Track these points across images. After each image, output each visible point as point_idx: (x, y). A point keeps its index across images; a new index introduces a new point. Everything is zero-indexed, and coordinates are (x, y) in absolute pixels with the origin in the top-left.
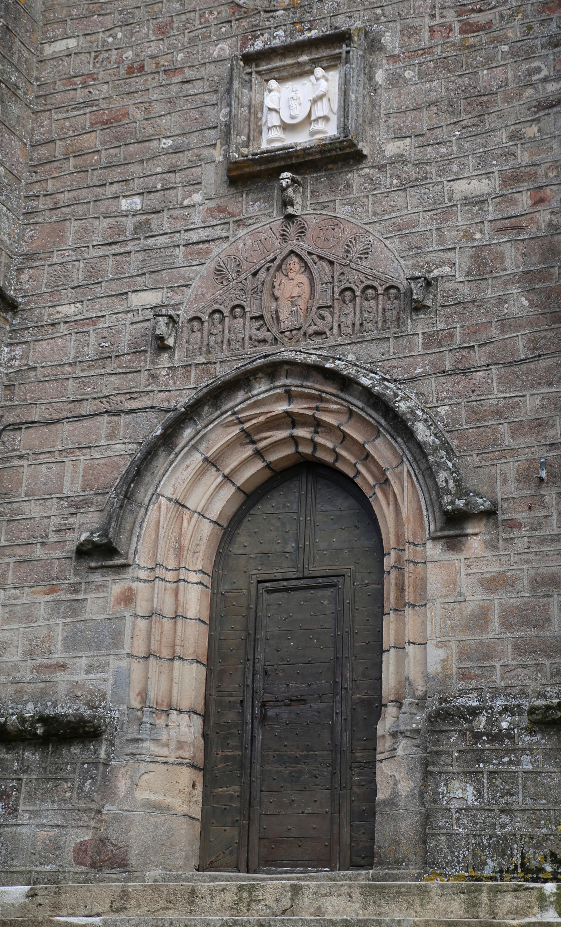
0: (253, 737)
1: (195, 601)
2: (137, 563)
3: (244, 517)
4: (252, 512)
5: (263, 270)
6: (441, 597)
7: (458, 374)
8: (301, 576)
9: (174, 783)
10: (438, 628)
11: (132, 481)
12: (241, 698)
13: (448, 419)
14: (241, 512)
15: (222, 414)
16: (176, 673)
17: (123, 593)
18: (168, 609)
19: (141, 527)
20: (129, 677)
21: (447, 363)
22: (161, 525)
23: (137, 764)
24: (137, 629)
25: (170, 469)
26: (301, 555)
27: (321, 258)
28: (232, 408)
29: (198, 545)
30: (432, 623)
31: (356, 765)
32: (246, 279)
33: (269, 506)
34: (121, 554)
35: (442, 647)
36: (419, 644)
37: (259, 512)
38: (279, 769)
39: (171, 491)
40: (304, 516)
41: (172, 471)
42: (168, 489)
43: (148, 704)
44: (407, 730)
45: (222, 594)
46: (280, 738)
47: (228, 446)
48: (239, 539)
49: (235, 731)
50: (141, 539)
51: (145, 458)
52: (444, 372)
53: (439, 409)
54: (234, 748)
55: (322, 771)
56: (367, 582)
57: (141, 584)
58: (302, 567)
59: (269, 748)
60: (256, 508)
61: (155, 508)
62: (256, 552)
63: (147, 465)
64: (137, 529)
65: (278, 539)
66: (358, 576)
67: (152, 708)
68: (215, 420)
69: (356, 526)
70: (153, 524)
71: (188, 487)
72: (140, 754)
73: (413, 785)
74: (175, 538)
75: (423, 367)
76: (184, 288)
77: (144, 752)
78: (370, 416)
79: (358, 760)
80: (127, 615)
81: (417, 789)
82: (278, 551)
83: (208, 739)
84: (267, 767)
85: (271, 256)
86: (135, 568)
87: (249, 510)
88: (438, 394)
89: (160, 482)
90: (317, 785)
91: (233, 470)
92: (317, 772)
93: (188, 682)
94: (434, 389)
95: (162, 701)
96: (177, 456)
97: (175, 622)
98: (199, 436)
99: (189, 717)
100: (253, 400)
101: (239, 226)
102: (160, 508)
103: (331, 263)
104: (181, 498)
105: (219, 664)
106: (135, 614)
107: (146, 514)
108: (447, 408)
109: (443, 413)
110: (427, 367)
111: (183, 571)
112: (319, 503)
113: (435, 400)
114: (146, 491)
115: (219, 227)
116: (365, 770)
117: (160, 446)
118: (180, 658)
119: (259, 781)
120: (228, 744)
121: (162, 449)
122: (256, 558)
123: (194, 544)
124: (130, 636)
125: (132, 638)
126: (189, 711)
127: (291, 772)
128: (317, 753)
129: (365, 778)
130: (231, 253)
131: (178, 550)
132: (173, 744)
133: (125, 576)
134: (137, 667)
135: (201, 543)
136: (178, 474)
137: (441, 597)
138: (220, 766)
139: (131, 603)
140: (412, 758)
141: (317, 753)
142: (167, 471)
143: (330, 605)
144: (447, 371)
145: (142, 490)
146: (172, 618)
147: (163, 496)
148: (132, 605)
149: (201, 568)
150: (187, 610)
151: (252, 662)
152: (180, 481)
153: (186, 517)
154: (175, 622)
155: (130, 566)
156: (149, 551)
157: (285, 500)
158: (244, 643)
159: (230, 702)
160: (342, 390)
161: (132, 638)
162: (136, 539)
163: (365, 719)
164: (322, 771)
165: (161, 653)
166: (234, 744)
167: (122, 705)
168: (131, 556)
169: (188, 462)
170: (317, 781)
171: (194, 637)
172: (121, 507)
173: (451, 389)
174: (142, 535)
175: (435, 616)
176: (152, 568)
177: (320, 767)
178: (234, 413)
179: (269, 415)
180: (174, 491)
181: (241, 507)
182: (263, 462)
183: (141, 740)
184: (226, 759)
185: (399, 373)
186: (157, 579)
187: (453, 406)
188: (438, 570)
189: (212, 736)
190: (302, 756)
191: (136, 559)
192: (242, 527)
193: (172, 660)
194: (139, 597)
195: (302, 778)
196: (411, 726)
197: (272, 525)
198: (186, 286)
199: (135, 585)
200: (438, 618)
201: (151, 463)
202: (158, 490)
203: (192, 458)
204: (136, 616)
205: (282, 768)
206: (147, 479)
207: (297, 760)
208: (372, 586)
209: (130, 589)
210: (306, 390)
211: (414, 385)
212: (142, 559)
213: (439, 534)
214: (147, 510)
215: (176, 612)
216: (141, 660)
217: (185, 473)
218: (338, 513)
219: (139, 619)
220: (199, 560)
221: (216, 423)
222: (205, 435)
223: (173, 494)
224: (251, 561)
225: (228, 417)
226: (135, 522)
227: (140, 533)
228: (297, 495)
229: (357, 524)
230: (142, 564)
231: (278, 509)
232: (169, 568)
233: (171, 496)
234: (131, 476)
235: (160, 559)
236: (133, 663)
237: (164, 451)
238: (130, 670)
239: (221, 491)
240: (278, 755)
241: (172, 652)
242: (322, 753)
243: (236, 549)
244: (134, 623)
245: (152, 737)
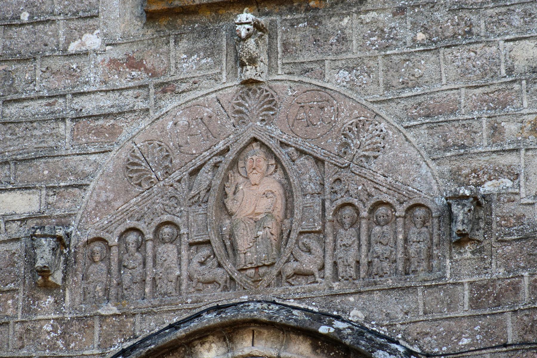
5: (208, 167)
7: (527, 350)
21: (510, 331)
27: (302, 153)
32: (179, 181)
52: (505, 345)
75: (472, 336)
76: (77, 191)
85: (221, 146)
101: (164, 92)
103: (318, 161)
110: (478, 337)
115: (130, 92)
130: (154, 136)
144: (511, 345)
198: (80, 186)
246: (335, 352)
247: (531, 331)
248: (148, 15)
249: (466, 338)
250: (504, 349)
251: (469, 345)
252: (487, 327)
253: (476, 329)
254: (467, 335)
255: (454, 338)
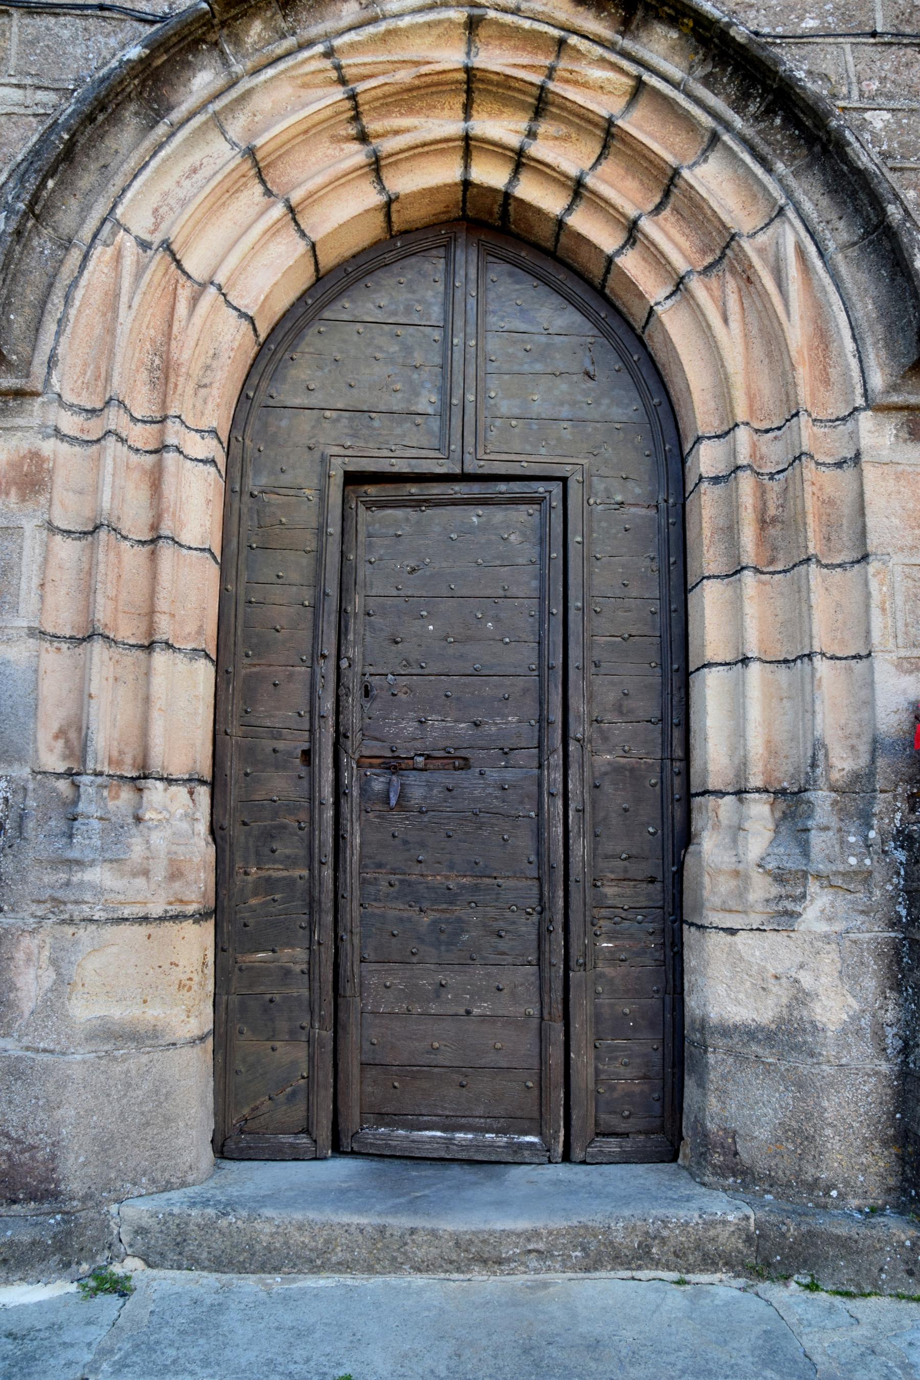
0: (338, 837)
1: (196, 503)
2: (57, 389)
3: (307, 325)
4: (327, 314)
6: (902, 549)
7: (906, 45)
8: (458, 471)
9: (166, 966)
10: (900, 624)
11: (51, 173)
12: (306, 746)
13: (890, 140)
14: (301, 310)
15: (301, 47)
16: (159, 683)
17: (15, 465)
18: (134, 517)
19: (68, 299)
20: (36, 688)
21: (879, 16)
22: (124, 299)
23: (70, 930)
24: (53, 562)
25: (154, 164)
26: (456, 422)
28: (327, 36)
29: (208, 368)
30: (883, 610)
31: (604, 912)
33: (370, 306)
34: (10, 364)
35: (911, 672)
36: (831, 658)
37: (345, 317)
38: (405, 915)
39: (149, 222)
40: (462, 335)
41: (157, 171)
42: (138, 214)
43: (90, 765)
44: (836, 873)
45: (252, 495)
46: (405, 842)
47: (306, 132)
48: (293, 372)
49: (290, 821)
50: (68, 330)
51: (90, 118)
52: (874, 34)
53: (868, 115)
54: (290, 862)
55: (514, 923)
56: (619, 498)
57: (64, 447)
58: (459, 450)
59: (380, 865)
60: (337, 306)
61: (107, 257)
62: (340, 406)
63: (92, 143)
64: (57, 299)
65: (394, 382)
66: (599, 485)
67: (100, 774)
68: (280, 58)
69: (587, 374)
70: (96, 298)
71: (198, 215)
72: (76, 902)
73: (856, 1006)
74: (153, 341)
75: (821, 16)
77: (88, 897)
78: (698, 102)
79: (610, 902)
80: (29, 526)
81: (868, 1016)
82: (395, 408)
83: (223, 838)
84: (375, 908)
86: (50, 402)
87: (322, 308)
88: (859, 82)
89: (124, 191)
90: (504, 954)
91: (310, 195)
92: (501, 924)
93: (182, 705)
94: (852, 70)
95: (121, 752)
96: (173, 134)
97: (153, 553)
98: (234, 93)
99: (191, 793)
100: (383, 27)
102: (118, 257)
104: (180, 240)
105: (246, 661)
106: (50, 523)
107: (82, 267)
108: (887, 116)
109: (879, 125)
110: (830, 19)
111: (172, 426)
112: (494, 312)
113: (855, 94)
114: (85, 210)
116: (626, 924)
117: (129, 98)
118: (169, 646)
119: (356, 941)
120: (273, 851)
121: (133, 107)
122: (338, 420)
123: (200, 364)
124: (36, 581)
125: (42, 585)
126: (190, 780)
127: (434, 922)
128: (500, 881)
129: (627, 943)
131: (158, 374)
132: (159, 872)
133: (19, 421)
134: (55, 663)
135: (215, 364)
136: (167, 184)
137: (902, 549)
138: (253, 901)
139: (38, 492)
140: (855, 942)
141: (500, 881)
142: (143, 168)
143: (526, 546)
144: (882, 34)
145: (74, 204)
146: (143, 543)
147: (127, 230)
148: (42, 500)
149: (215, 424)
150: (182, 525)
151: (332, 661)
152: (172, 202)
153: (184, 295)
154: (153, 553)
155: (35, 394)
156: (85, 364)
157: (410, 296)
158: (310, 616)
159: (274, 751)
160: (623, 34)
161: (42, 585)
162: (53, 327)
163: (626, 810)
164: (514, 923)
165: (116, 630)
166: (288, 851)
167: (16, 766)
168: (39, 368)
169: (195, 158)
170: (503, 945)
171: (191, 592)
172: (18, 233)
173: (893, 77)
174: (72, 318)
175: (893, 595)
176: (93, 411)
177: (508, 914)
178: (329, 54)
179: (425, 69)
180: (157, 226)
181: (301, 298)
182: (380, 192)
183: (79, 863)
184: (268, 885)
185: (763, 20)
186: (112, 439)
187: (900, 114)
188: (891, 484)
189: (237, 832)
190: (463, 887)
191: (54, 380)
192: (303, 347)
193: (149, 648)
194: (59, 480)
195: (465, 937)
196: (845, 862)
197: (380, 349)
199: (49, 447)
200: (899, 600)
201: (102, 137)
202: (119, 211)
203: (207, 150)
204: (51, 528)
205: (413, 913)
206: (86, 180)
207: (450, 897)
208: (633, 510)
209: (35, 456)
210: (527, 24)
211: (803, 53)
212: (67, 381)
213: (896, 399)
214: (86, 257)
215: (154, 527)
216: (64, 646)
217: (186, 183)
218: (543, 339)
219: (58, 538)
220: (210, 406)
221: (282, 66)
222: (249, 93)
223: (152, 232)
224: (326, 425)
225: (311, 61)
226: (51, 285)
227: (65, 315)
228: (440, 287)
229: (591, 369)
230: (68, 397)
231: (394, 313)
232: (136, 415)
233: (147, 237)
234: (50, 156)
235: (118, 386)
236: (44, 654)
237: (137, 114)
238: (36, 671)
239: (271, 246)
240: (401, 882)
241: (144, 627)
242: (511, 883)
243: (288, 393)
244: (46, 547)
245: (107, 856)
246: (609, 11)
247: (908, 22)
248: (782, 806)
249: (812, 18)
250: (872, 40)
251: (817, 28)
252: (844, 6)
253: (827, 7)
254: (813, 15)
255: (793, 17)
